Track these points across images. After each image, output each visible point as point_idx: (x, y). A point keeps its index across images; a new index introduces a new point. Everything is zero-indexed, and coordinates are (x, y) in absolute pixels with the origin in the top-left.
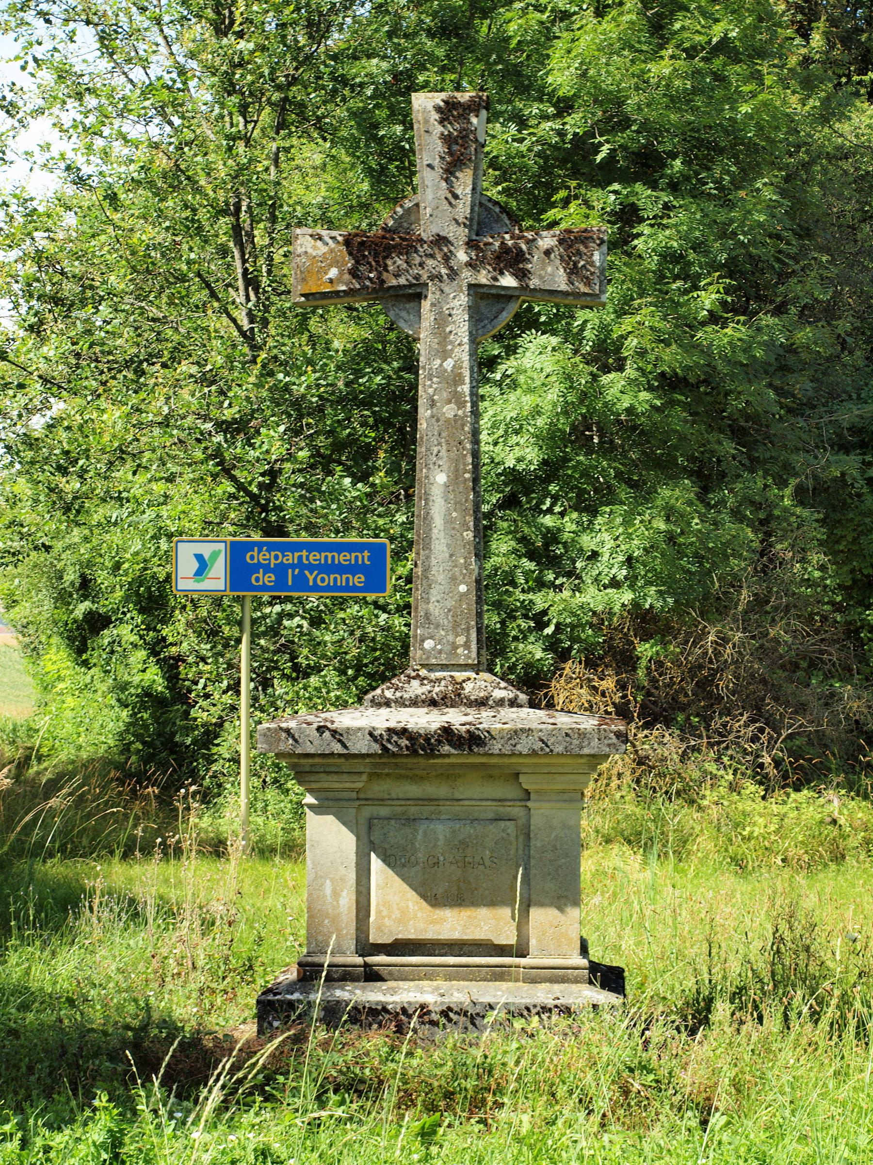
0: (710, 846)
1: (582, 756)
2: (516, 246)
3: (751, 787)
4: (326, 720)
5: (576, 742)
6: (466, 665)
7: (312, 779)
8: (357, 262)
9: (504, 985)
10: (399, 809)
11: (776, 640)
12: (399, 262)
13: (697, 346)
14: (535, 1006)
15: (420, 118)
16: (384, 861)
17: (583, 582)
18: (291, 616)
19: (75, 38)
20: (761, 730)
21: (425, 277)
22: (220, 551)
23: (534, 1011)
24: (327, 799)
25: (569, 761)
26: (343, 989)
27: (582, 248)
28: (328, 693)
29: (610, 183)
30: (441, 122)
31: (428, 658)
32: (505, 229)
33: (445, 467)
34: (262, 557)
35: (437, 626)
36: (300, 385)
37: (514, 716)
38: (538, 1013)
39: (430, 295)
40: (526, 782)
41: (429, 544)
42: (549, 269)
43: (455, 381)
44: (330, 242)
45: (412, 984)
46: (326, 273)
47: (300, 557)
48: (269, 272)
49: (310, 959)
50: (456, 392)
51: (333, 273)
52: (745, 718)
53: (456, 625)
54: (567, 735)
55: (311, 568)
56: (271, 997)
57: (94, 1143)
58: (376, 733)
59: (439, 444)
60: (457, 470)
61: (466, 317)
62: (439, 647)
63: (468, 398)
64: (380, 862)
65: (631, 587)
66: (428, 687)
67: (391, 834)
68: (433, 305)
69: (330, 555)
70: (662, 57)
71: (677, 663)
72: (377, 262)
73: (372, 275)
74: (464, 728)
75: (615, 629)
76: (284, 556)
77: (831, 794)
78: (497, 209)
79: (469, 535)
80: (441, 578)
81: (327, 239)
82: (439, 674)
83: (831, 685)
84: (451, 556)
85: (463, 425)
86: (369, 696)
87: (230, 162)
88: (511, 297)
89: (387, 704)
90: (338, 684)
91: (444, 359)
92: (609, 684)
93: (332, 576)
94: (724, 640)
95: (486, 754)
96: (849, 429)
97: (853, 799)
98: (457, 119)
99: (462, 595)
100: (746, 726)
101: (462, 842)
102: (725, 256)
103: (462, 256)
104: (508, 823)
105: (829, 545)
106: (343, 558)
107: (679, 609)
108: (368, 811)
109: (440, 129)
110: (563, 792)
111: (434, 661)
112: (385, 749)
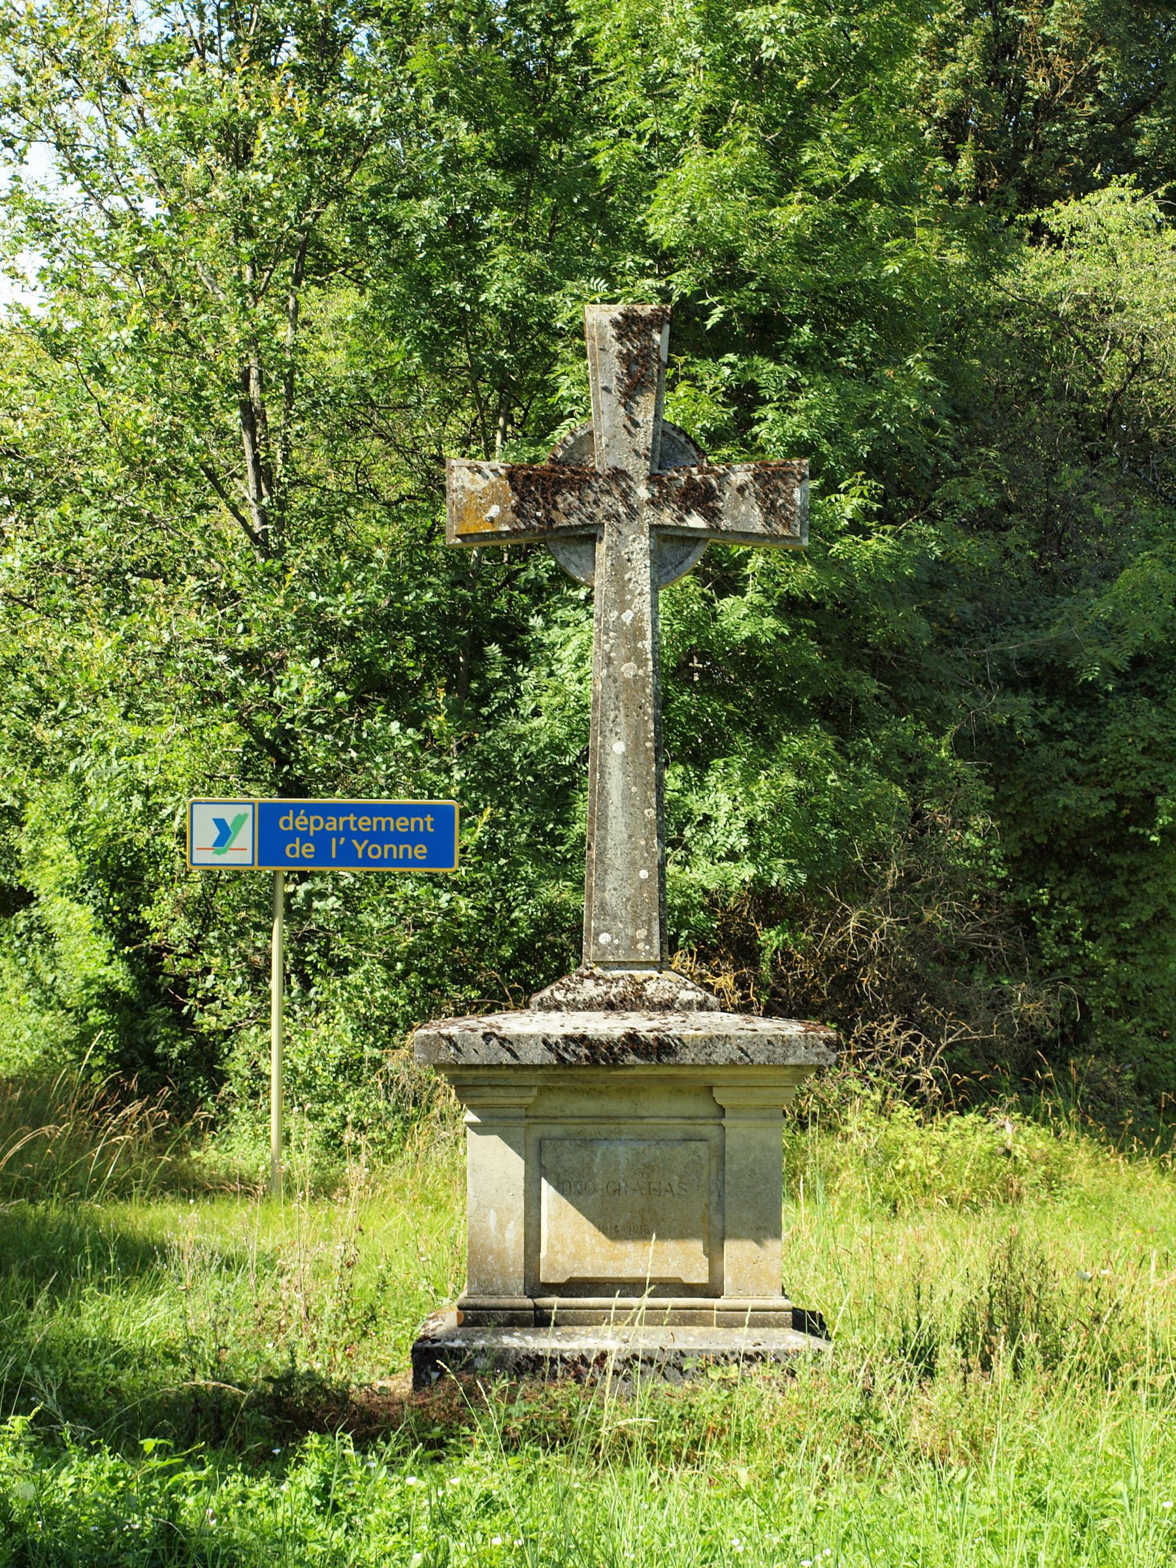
0: (857, 1183)
1: (785, 1067)
2: (705, 481)
3: (903, 1111)
4: (491, 1026)
5: (780, 1051)
6: (647, 963)
7: (475, 1093)
8: (522, 499)
9: (697, 1330)
10: (574, 1128)
11: (931, 927)
12: (571, 499)
13: (836, 562)
14: (733, 1353)
15: (595, 333)
16: (556, 1188)
17: (692, 853)
18: (322, 895)
19: (25, 158)
20: (916, 1039)
21: (600, 516)
22: (246, 815)
23: (732, 1359)
24: (491, 1117)
25: (771, 1072)
26: (511, 1335)
27: (780, 484)
28: (372, 992)
29: (722, 355)
30: (619, 338)
31: (603, 954)
32: (692, 462)
33: (623, 735)
34: (299, 822)
35: (614, 918)
36: (337, 607)
37: (706, 1021)
38: (737, 1361)
39: (605, 538)
40: (721, 1096)
41: (605, 823)
42: (743, 508)
43: (634, 635)
44: (491, 475)
45: (589, 1329)
46: (486, 511)
47: (347, 823)
48: (285, 459)
49: (471, 1301)
50: (636, 648)
51: (494, 511)
52: (894, 1024)
53: (636, 917)
54: (769, 1042)
55: (360, 836)
56: (429, 1344)
57: (307, 1488)
58: (550, 1041)
59: (617, 708)
60: (637, 739)
61: (648, 563)
62: (616, 942)
63: (649, 656)
64: (552, 1188)
65: (752, 859)
66: (604, 988)
67: (565, 1157)
68: (609, 548)
69: (384, 821)
70: (790, 203)
71: (809, 954)
72: (545, 499)
73: (539, 514)
74: (651, 1035)
75: (733, 912)
76: (326, 821)
77: (1001, 1118)
78: (683, 439)
79: (651, 813)
80: (618, 862)
81: (487, 472)
82: (617, 973)
83: (998, 982)
84: (630, 837)
85: (644, 687)
86: (536, 998)
87: (246, 325)
88: (699, 539)
89: (558, 1007)
90: (384, 982)
91: (622, 611)
92: (726, 981)
93: (386, 847)
94: (868, 926)
95: (678, 1065)
96: (1018, 661)
97: (1029, 1125)
98: (637, 335)
99: (643, 882)
100: (898, 1033)
101: (646, 1166)
102: (867, 448)
103: (643, 493)
104: (699, 1144)
105: (993, 808)
106: (401, 824)
107: (814, 887)
108: (538, 1131)
109: (618, 346)
110: (763, 1108)
111: (610, 958)
112: (561, 1059)
